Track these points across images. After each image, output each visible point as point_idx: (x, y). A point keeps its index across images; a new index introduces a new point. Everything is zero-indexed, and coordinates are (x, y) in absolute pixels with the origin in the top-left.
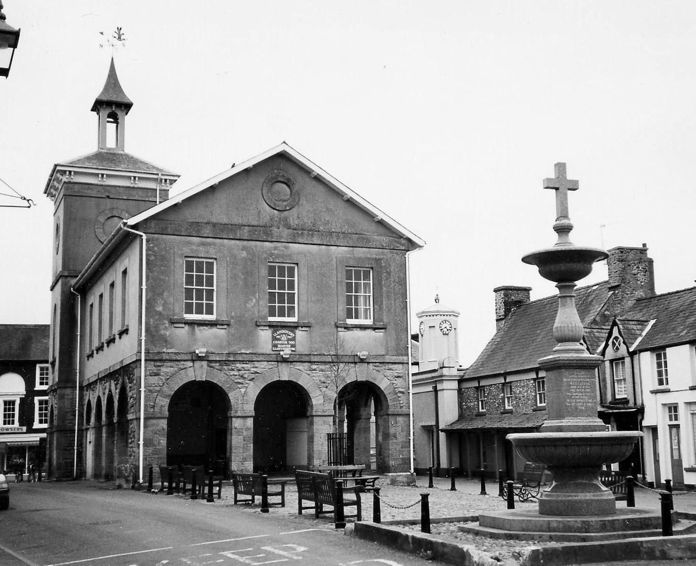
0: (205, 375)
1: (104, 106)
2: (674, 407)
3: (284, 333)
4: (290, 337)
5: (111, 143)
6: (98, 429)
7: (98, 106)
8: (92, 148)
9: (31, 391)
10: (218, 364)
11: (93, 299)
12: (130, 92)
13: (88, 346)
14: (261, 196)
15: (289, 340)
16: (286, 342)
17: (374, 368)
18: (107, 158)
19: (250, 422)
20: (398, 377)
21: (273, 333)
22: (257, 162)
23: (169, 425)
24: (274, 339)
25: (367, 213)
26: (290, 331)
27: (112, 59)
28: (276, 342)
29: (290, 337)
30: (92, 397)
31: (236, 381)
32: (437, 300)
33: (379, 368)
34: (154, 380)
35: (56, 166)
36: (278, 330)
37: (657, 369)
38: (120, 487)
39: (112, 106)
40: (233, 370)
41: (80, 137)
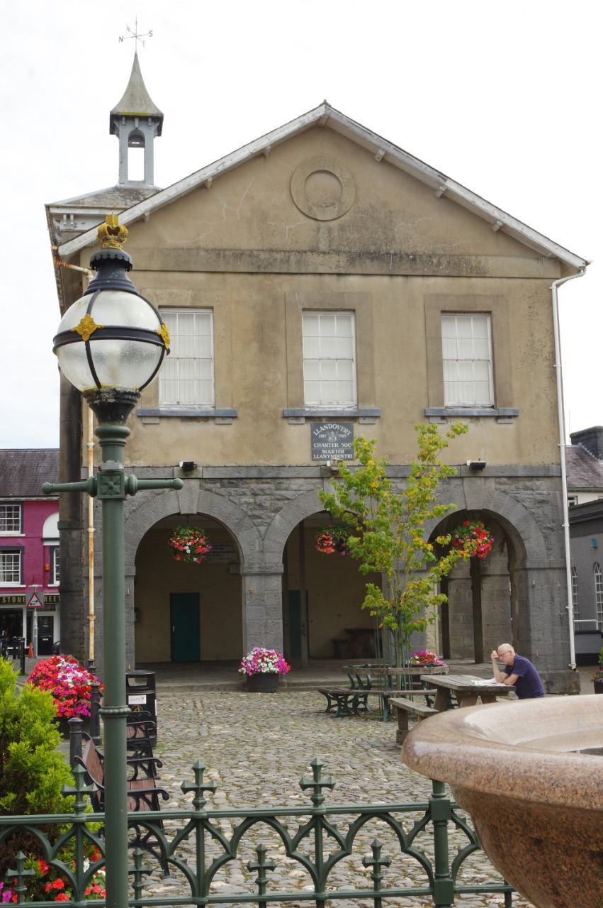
0: (196, 504)
1: (123, 122)
3: (332, 430)
4: (343, 436)
7: (116, 120)
8: (112, 181)
10: (218, 485)
12: (160, 99)
14: (325, 223)
15: (340, 441)
16: (336, 445)
17: (498, 486)
19: (276, 584)
20: (542, 502)
21: (313, 429)
22: (141, 68)
24: (314, 439)
25: (456, 203)
26: (340, 424)
27: (136, 55)
28: (319, 445)
29: (343, 436)
31: (250, 513)
33: (506, 487)
36: (322, 425)
37: (13, 582)
40: (244, 494)
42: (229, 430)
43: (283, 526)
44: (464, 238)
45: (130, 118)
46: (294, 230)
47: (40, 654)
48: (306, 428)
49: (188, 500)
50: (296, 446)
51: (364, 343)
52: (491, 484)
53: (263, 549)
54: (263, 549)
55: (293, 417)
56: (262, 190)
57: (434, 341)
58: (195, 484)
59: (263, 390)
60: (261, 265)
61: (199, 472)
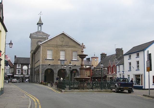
2: (141, 75)
5: (40, 30)
6: (36, 75)
7: (38, 24)
8: (37, 31)
9: (28, 69)
11: (36, 55)
13: (38, 59)
18: (39, 32)
19: (57, 75)
23: (45, 75)
24: (61, 62)
30: (35, 70)
32: (94, 55)
34: (42, 68)
35: (31, 34)
38: (38, 84)
39: (40, 24)
41: (35, 29)
42: (53, 61)
43: (58, 70)
44: (75, 44)
45: (40, 24)
46: (60, 43)
47: (90, 58)
48: (60, 61)
49: (49, 67)
50: (59, 63)
51: (66, 54)
52: (76, 67)
53: (56, 72)
54: (56, 72)
55: (59, 60)
56: (58, 40)
57: (72, 54)
58: (50, 66)
59: (56, 57)
60: (57, 46)
61: (51, 65)
